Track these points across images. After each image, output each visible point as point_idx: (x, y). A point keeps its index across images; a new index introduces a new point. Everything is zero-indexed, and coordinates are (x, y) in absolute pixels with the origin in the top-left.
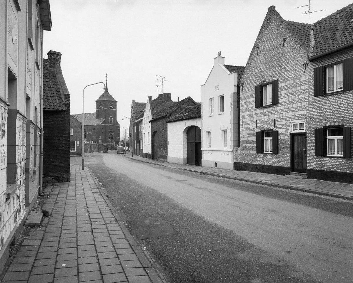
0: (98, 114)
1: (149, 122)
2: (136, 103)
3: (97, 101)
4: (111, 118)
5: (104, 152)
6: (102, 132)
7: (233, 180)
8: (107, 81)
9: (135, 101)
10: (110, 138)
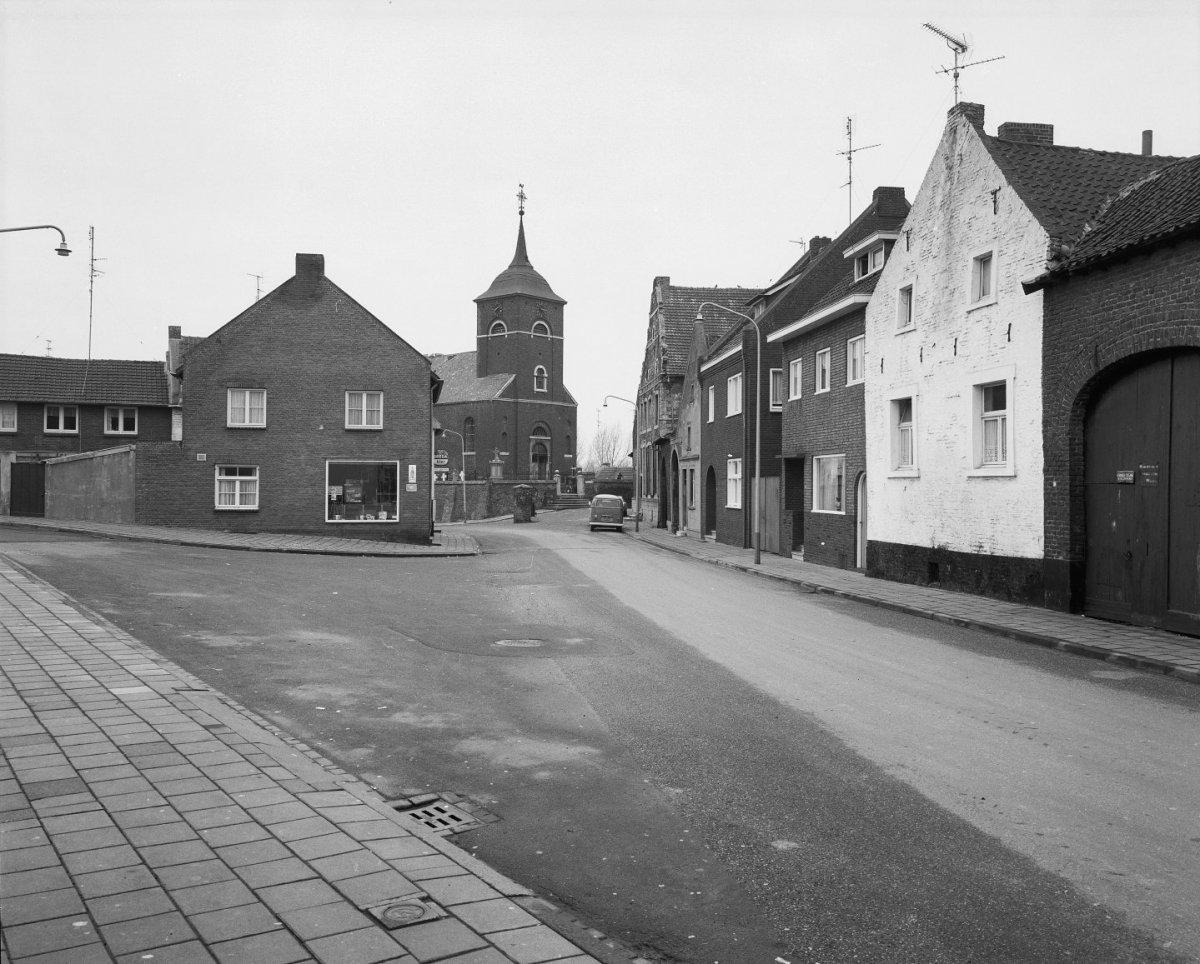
0: (488, 358)
1: (1029, 288)
2: (673, 288)
3: (481, 302)
4: (540, 371)
5: (517, 521)
6: (504, 434)
8: (522, 213)
10: (534, 460)
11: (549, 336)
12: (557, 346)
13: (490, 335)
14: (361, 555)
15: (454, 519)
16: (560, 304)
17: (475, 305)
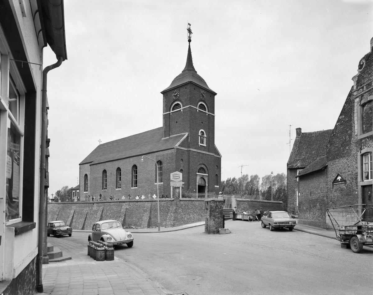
7: (64, 52)
8: (190, 41)
9: (300, 129)
11: (207, 112)
12: (211, 120)
13: (171, 111)
14: (307, 232)
15: (149, 226)
16: (213, 94)
17: (162, 95)
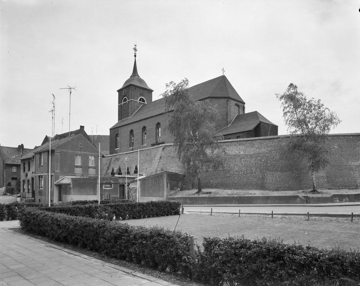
8: (135, 56)
